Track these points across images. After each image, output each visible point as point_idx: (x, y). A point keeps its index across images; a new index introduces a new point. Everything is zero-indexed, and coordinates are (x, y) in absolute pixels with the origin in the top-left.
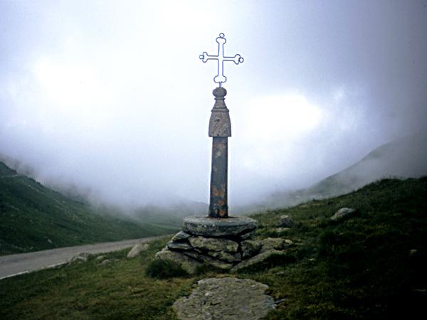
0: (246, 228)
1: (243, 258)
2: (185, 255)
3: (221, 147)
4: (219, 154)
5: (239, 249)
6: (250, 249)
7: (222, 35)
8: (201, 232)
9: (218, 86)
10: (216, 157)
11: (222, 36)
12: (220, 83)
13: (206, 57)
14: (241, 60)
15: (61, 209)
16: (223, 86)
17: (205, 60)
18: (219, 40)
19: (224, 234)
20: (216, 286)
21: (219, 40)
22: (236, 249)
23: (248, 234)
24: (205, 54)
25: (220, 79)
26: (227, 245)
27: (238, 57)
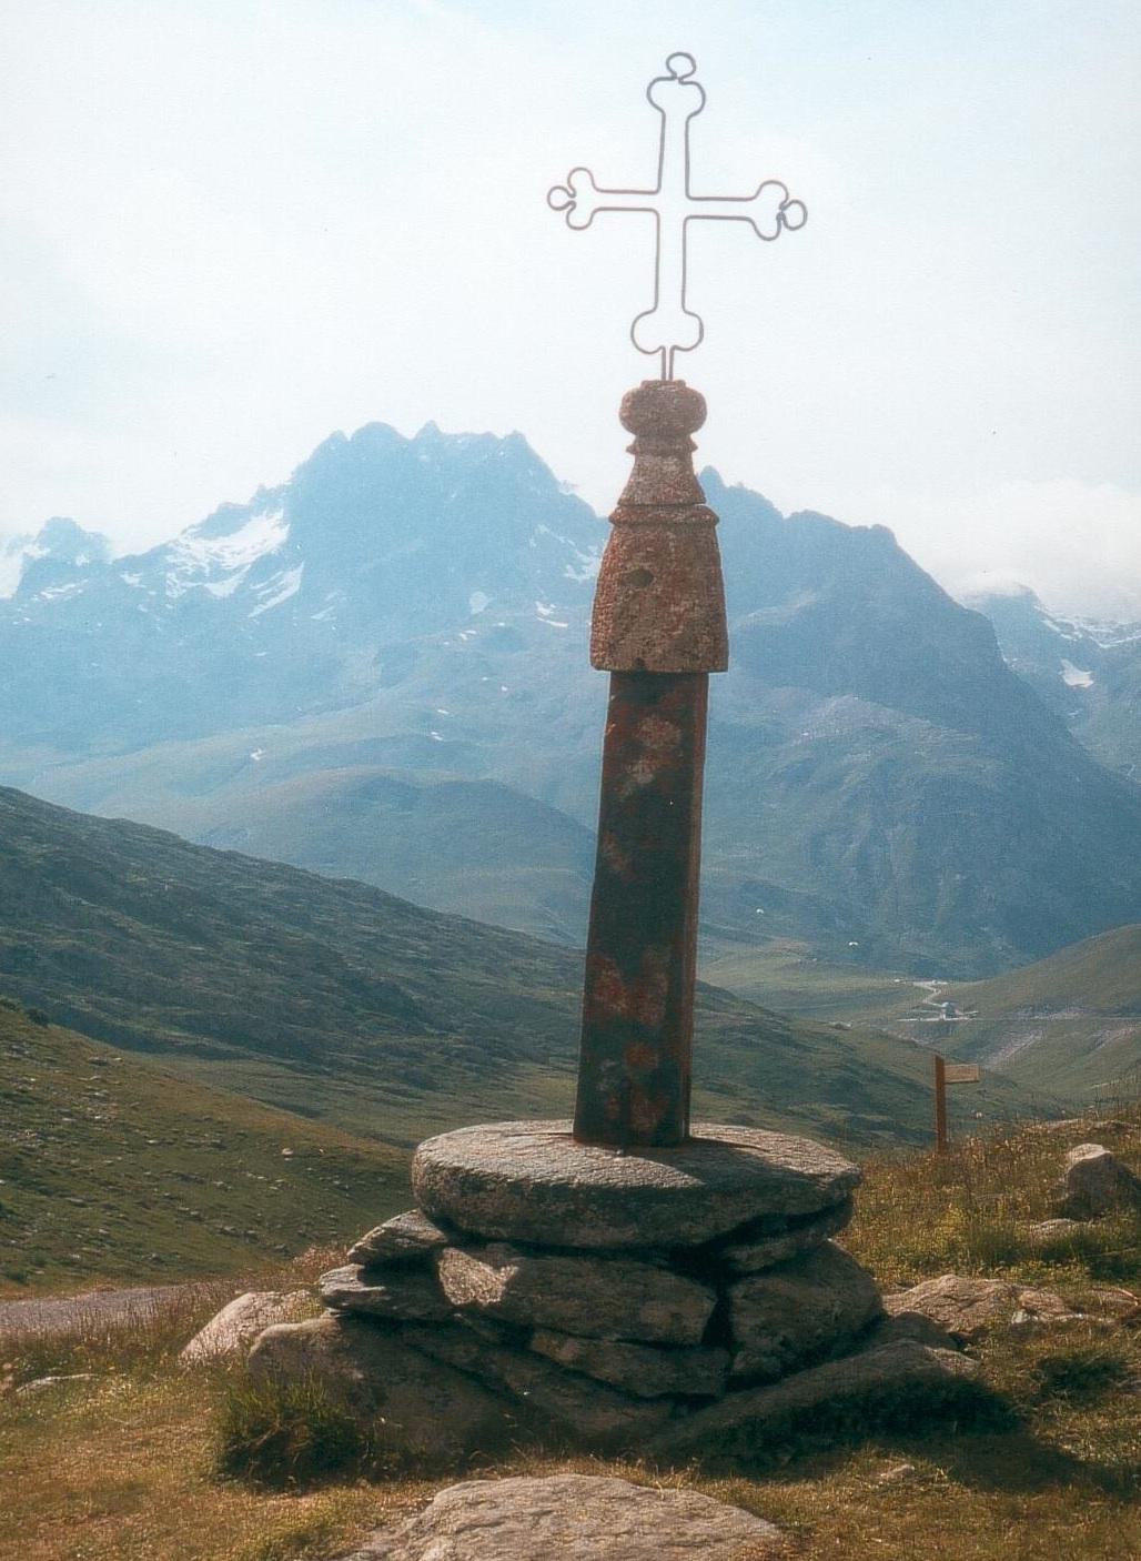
0: (760, 1207)
1: (736, 1383)
2: (416, 1348)
3: (656, 732)
4: (642, 774)
5: (719, 1332)
6: (788, 1332)
7: (681, 66)
8: (499, 1220)
9: (653, 373)
10: (628, 790)
11: (680, 72)
12: (668, 354)
13: (587, 199)
14: (794, 215)
15: (390, 1171)
16: (688, 372)
17: (579, 217)
18: (667, 93)
19: (628, 1234)
20: (494, 1514)
21: (664, 92)
22: (695, 1325)
23: (779, 1247)
24: (580, 181)
25: (669, 327)
26: (645, 1297)
27: (773, 196)
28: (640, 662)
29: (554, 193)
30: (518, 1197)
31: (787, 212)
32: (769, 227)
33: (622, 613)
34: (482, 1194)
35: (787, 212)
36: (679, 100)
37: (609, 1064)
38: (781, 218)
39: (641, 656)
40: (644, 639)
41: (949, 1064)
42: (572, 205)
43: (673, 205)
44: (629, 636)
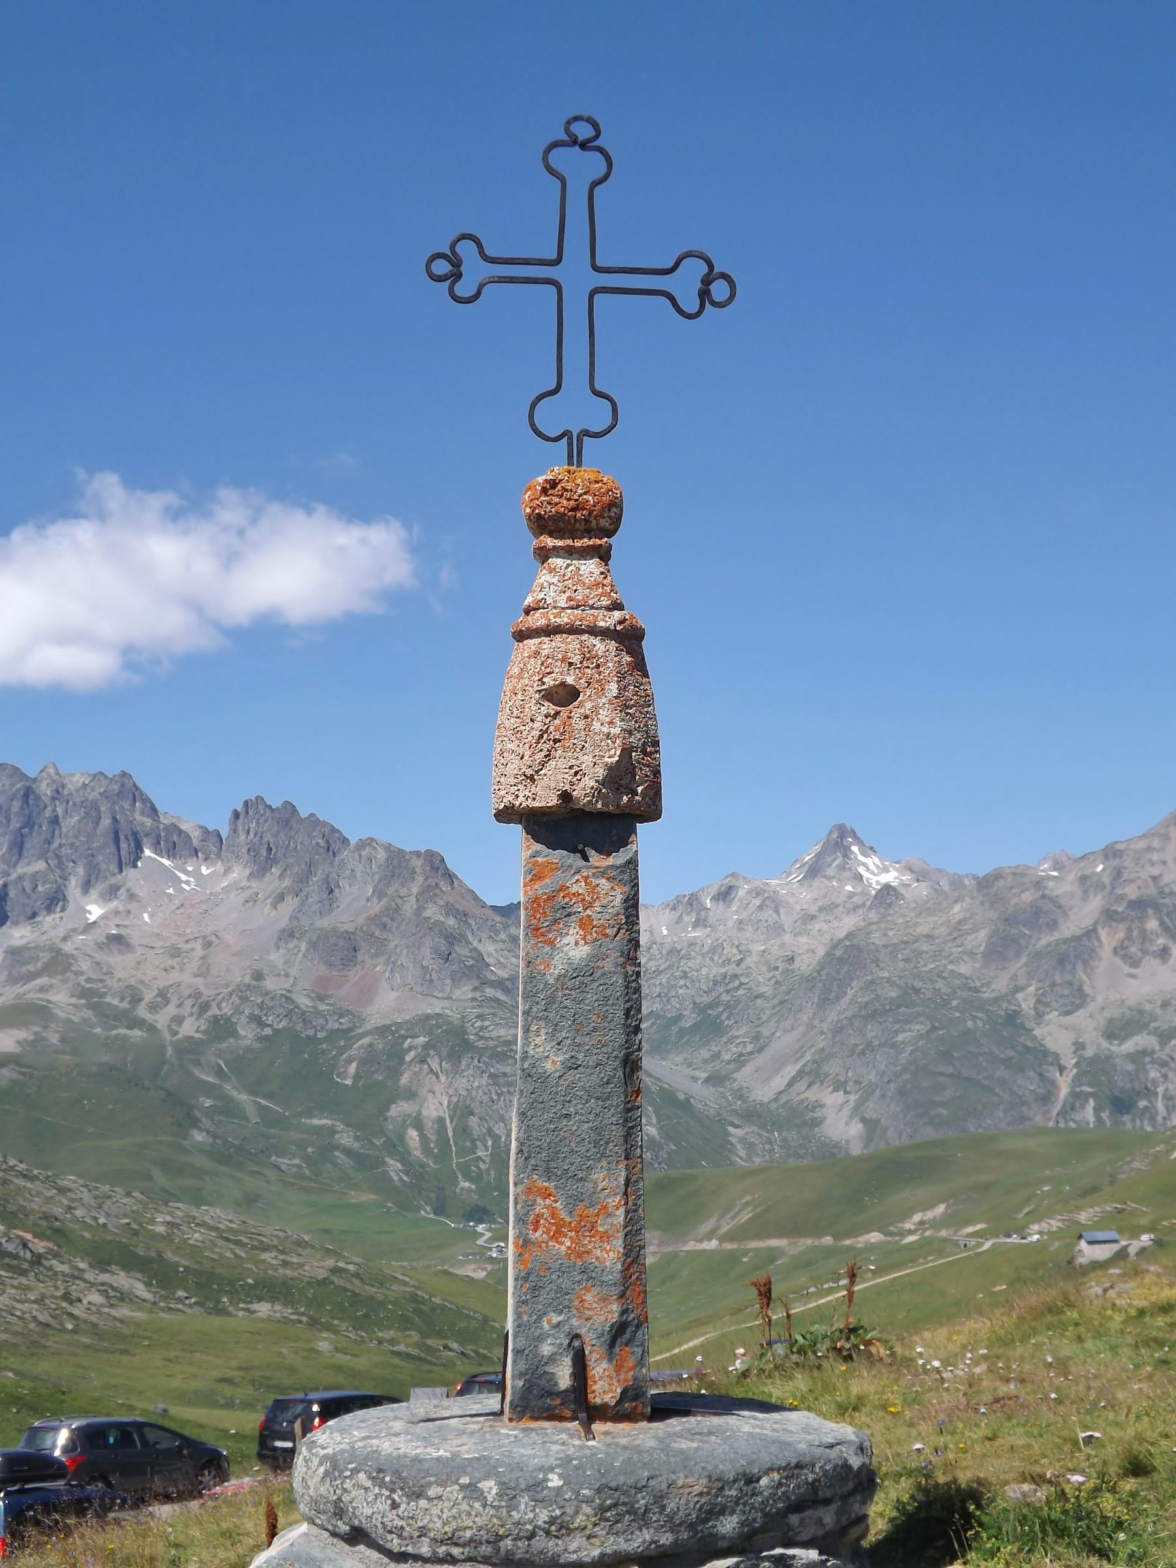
14: (719, 290)
17: (464, 288)
21: (563, 159)
24: (466, 250)
28: (565, 796)
29: (608, 422)
30: (477, 1505)
31: (581, 138)
32: (690, 303)
33: (541, 737)
34: (423, 1503)
35: (581, 138)
36: (580, 167)
37: (556, 1319)
38: (704, 294)
39: (567, 787)
40: (571, 767)
41: (240, 1437)
42: (456, 276)
43: (576, 276)
44: (552, 763)
